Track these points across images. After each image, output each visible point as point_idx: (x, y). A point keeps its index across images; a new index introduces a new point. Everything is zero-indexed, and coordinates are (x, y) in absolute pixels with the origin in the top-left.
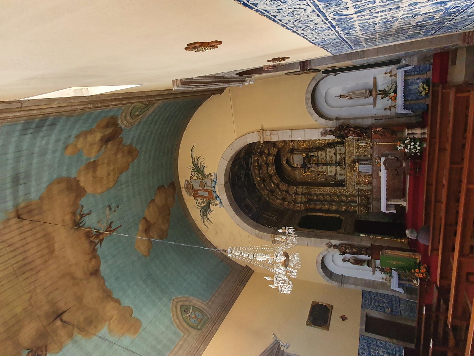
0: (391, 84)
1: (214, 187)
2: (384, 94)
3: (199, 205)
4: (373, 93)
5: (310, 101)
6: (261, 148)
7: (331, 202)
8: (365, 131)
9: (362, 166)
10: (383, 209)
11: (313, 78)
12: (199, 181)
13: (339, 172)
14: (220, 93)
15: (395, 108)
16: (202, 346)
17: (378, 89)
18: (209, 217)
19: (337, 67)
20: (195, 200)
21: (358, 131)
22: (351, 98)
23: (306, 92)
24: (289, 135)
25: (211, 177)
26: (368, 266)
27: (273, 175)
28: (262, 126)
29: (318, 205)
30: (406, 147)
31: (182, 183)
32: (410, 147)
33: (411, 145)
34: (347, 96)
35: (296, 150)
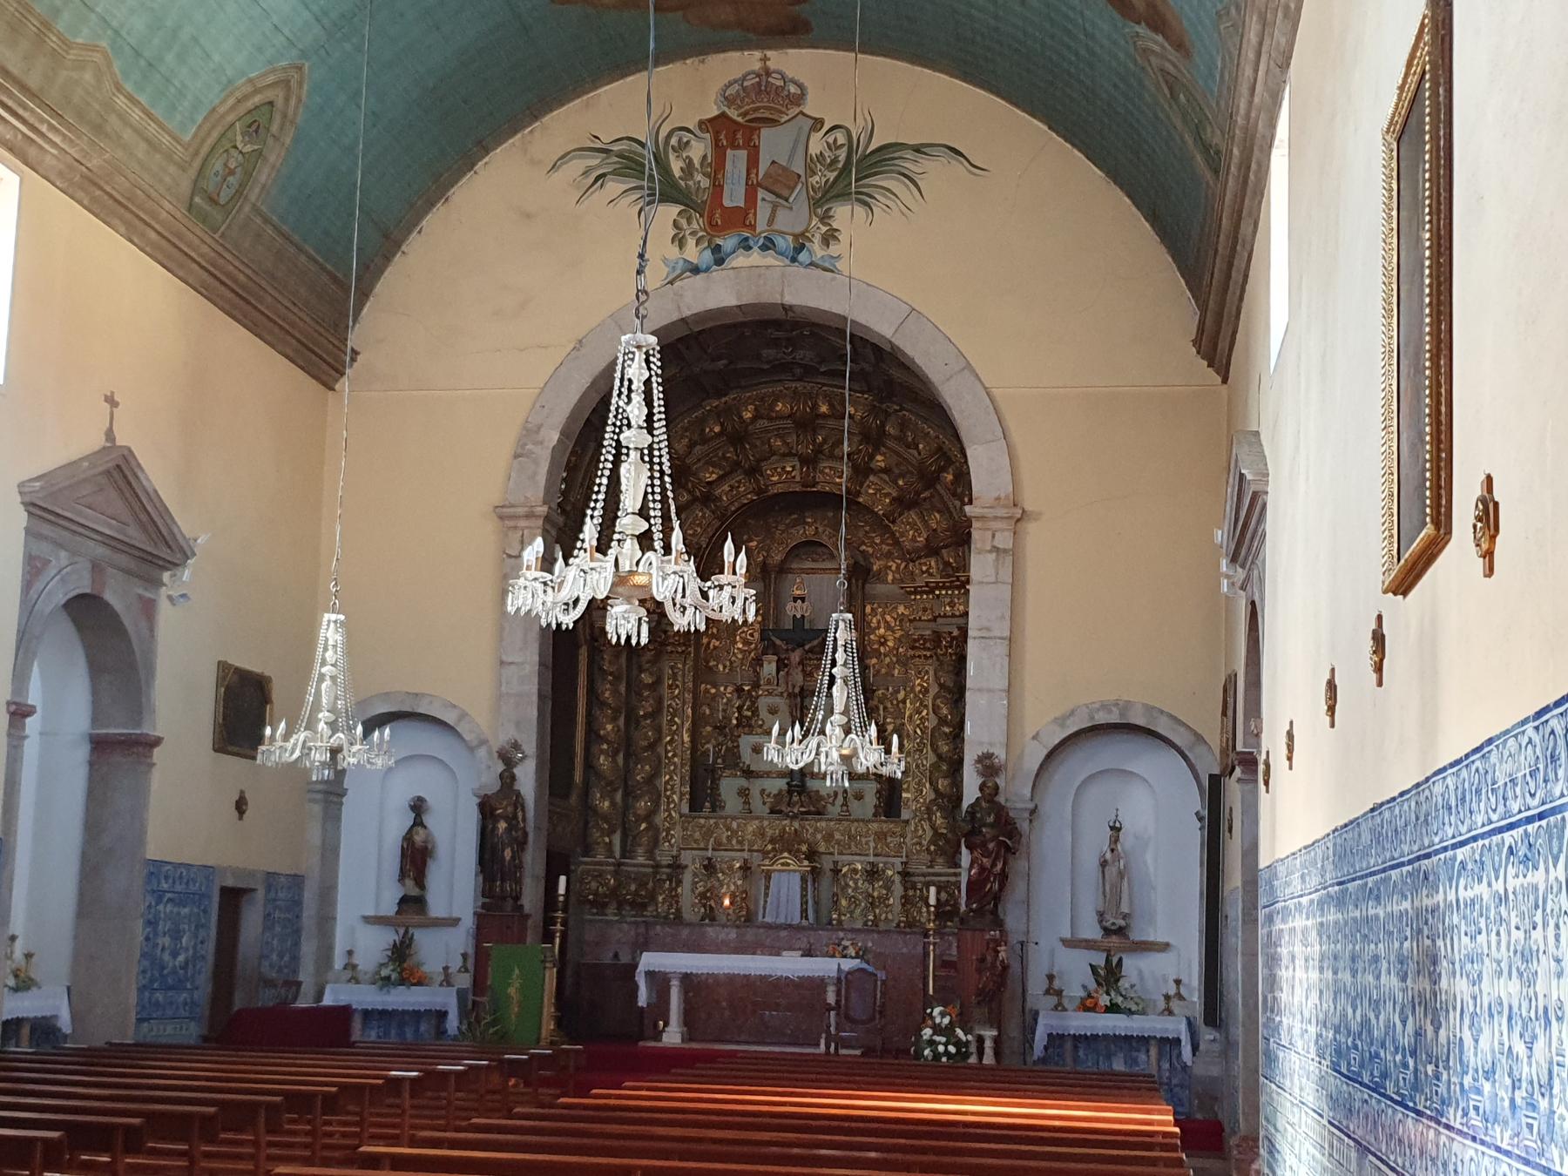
0: (1139, 997)
1: (768, 245)
2: (1109, 976)
3: (674, 141)
4: (1114, 938)
5: (1114, 718)
6: (900, 439)
7: (627, 746)
8: (987, 907)
9: (798, 889)
10: (650, 960)
11: (1199, 738)
12: (798, 167)
13: (756, 786)
14: (1197, 343)
15: (1056, 1008)
16: (153, 235)
17: (420, 930)
18: (614, 187)
19: (1227, 834)
20: (702, 124)
21: (989, 886)
22: (1104, 864)
23: (1153, 708)
24: (988, 629)
25: (817, 239)
26: (404, 901)
27: (757, 481)
28: (1037, 516)
29: (615, 692)
30: (937, 1029)
31: (793, 62)
32: (940, 1043)
33: (946, 1045)
34: (1112, 850)
35: (863, 588)
